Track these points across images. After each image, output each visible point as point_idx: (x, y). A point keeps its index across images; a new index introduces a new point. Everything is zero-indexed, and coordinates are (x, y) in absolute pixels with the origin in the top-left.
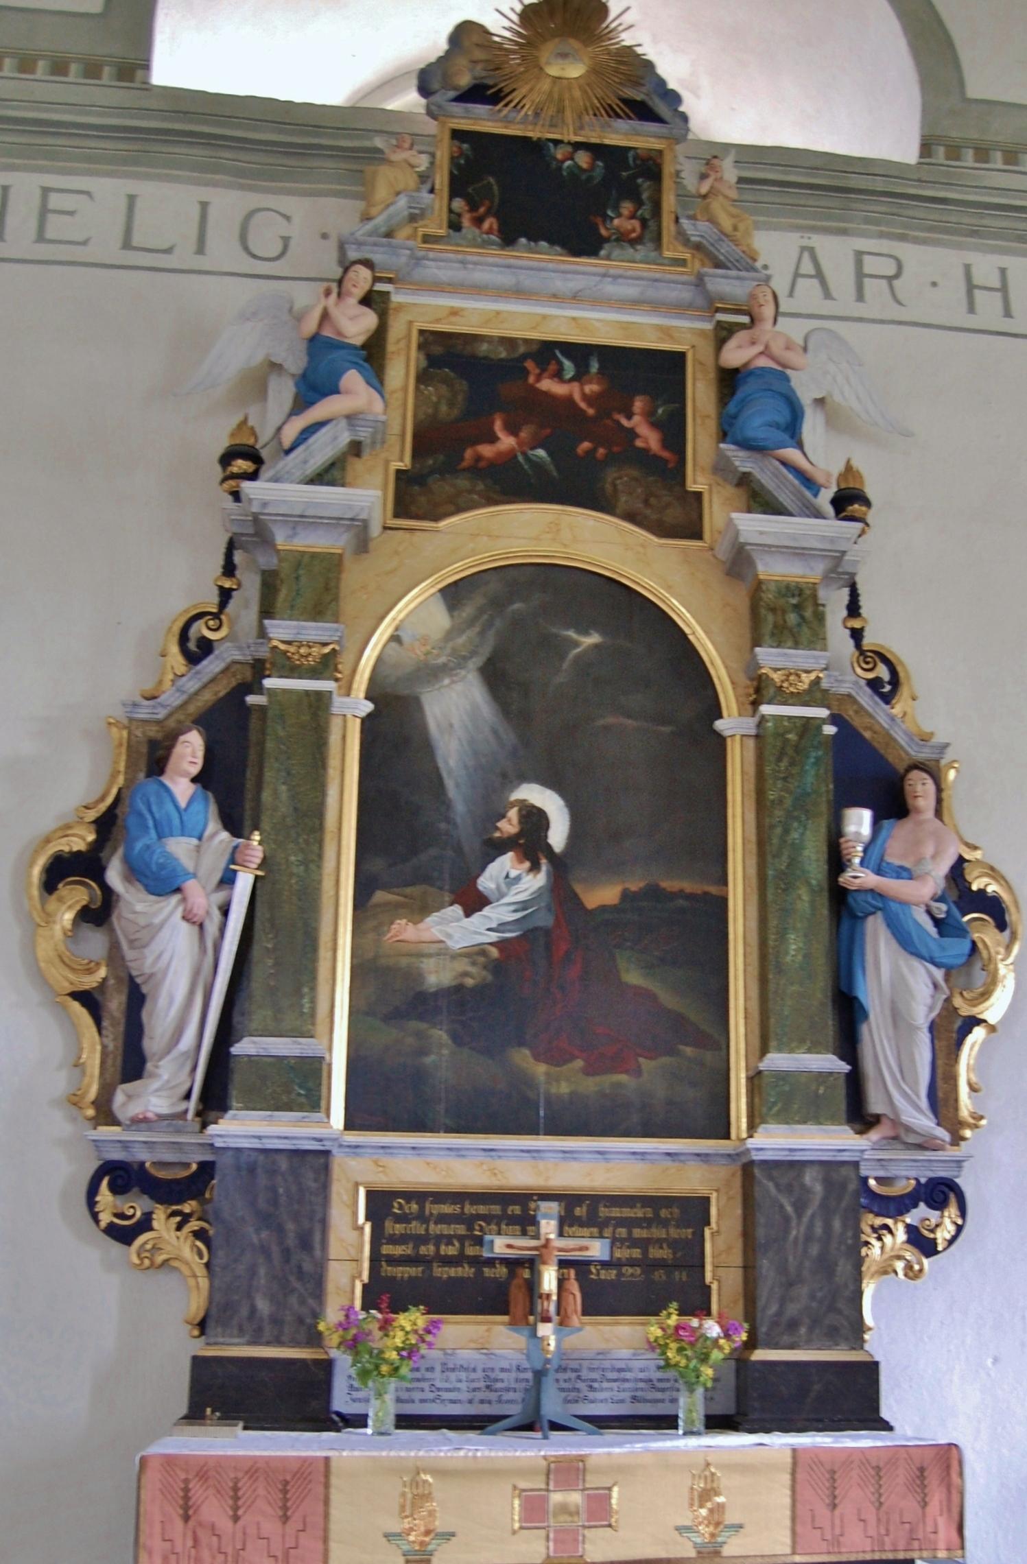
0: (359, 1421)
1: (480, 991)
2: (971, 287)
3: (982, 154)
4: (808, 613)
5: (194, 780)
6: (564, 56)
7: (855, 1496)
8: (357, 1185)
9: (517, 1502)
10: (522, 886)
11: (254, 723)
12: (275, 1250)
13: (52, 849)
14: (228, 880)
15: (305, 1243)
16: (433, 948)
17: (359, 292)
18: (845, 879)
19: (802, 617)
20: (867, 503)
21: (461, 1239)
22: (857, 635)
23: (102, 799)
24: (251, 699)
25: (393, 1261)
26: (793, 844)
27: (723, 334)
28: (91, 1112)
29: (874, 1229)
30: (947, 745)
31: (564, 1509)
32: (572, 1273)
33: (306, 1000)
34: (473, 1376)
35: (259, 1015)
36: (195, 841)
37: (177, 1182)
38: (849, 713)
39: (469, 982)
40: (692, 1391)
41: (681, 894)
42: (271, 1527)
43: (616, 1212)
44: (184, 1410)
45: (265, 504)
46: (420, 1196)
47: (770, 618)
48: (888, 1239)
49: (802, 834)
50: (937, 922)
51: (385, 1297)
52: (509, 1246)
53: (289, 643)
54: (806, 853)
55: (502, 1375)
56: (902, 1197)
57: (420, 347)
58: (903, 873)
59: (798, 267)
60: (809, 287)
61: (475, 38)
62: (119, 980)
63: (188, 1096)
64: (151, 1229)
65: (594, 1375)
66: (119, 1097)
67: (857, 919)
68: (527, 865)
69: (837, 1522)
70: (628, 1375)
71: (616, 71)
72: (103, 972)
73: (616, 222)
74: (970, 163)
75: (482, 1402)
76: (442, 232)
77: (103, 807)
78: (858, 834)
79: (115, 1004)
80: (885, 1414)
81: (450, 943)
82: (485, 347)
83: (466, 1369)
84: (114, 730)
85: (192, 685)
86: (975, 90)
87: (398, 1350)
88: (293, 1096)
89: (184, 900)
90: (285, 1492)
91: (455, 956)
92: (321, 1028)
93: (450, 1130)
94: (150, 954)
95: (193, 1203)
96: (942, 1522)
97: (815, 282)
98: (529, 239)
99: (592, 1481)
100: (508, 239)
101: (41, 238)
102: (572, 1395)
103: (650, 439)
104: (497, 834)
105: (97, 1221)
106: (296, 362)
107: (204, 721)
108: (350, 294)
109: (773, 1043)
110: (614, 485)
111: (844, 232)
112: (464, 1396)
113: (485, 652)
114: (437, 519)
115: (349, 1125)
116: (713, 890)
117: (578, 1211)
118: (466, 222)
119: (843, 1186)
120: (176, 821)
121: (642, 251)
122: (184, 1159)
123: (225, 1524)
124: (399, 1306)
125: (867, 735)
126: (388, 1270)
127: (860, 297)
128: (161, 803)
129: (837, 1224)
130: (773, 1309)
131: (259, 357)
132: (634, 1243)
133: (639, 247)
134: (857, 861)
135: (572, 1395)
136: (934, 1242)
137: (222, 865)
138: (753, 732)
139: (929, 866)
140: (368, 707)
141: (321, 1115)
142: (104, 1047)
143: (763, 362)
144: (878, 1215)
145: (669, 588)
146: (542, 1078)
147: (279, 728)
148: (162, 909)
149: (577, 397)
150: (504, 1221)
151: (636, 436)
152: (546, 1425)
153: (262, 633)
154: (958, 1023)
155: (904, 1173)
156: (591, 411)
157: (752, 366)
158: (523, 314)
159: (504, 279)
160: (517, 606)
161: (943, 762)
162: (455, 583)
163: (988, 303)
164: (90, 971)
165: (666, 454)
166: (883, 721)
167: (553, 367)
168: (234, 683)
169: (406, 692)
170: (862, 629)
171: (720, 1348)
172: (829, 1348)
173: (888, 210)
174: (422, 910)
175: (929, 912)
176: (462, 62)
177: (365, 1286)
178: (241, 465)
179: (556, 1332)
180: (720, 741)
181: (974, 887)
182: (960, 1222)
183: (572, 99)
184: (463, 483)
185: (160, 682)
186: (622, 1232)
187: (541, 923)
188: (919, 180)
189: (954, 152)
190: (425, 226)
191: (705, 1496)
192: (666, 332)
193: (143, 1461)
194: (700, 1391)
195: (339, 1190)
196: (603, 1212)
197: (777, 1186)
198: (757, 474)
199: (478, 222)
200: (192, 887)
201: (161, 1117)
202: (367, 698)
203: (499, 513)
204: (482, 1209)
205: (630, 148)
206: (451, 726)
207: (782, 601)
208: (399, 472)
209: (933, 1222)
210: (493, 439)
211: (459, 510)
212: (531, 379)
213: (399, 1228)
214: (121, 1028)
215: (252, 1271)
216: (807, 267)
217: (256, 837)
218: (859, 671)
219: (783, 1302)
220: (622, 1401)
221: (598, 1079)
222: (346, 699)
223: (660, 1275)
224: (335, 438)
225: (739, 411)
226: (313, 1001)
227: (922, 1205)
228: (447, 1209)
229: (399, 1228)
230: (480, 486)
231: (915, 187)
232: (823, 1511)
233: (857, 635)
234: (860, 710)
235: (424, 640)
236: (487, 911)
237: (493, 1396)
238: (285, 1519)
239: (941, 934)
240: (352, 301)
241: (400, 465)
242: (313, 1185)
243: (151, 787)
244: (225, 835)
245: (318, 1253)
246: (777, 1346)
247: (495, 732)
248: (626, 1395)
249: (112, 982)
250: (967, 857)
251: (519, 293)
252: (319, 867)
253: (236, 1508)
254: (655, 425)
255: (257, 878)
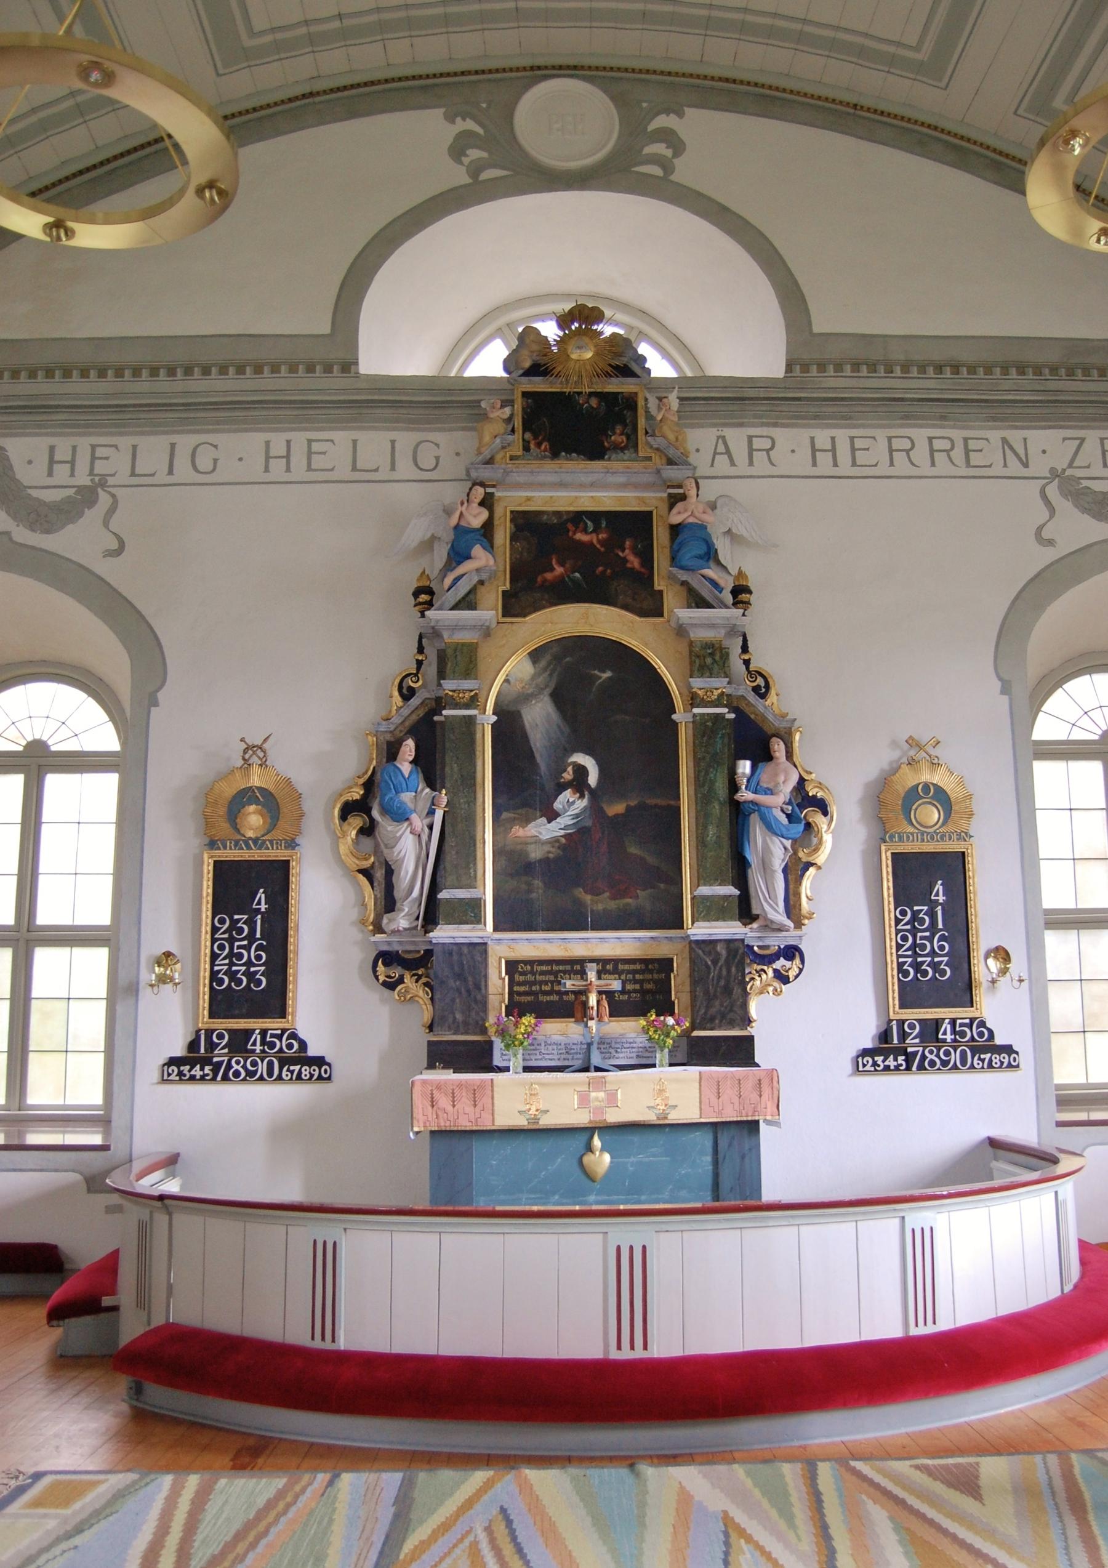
0: (507, 1069)
1: (557, 860)
2: (814, 450)
3: (822, 367)
4: (717, 658)
5: (411, 762)
6: (580, 348)
7: (729, 1093)
8: (500, 958)
9: (576, 1097)
10: (575, 806)
11: (438, 732)
12: (463, 990)
13: (343, 799)
14: (431, 813)
15: (478, 987)
16: (533, 840)
17: (478, 500)
18: (738, 797)
19: (714, 659)
20: (750, 592)
21: (552, 982)
22: (747, 663)
23: (366, 772)
24: (436, 718)
25: (519, 994)
26: (710, 780)
27: (675, 500)
28: (371, 928)
29: (757, 972)
30: (795, 719)
31: (597, 1099)
32: (604, 997)
33: (472, 871)
34: (560, 1047)
35: (451, 879)
36: (414, 794)
37: (414, 959)
38: (743, 706)
39: (551, 856)
40: (662, 1051)
41: (656, 806)
42: (469, 1109)
43: (627, 967)
44: (426, 1066)
45: (438, 621)
46: (530, 962)
47: (697, 661)
48: (764, 976)
49: (715, 775)
50: (788, 816)
51: (516, 1010)
52: (573, 985)
53: (454, 691)
54: (717, 784)
55: (574, 1047)
56: (771, 955)
57: (512, 520)
58: (770, 792)
59: (716, 449)
60: (722, 461)
61: (532, 337)
62: (380, 863)
63: (418, 918)
64: (404, 982)
65: (618, 1046)
66: (385, 921)
67: (746, 816)
68: (578, 795)
69: (721, 1104)
70: (634, 1045)
71: (609, 351)
72: (372, 859)
73: (613, 438)
74: (815, 374)
75: (564, 1059)
76: (520, 453)
77: (367, 777)
78: (744, 773)
79: (379, 874)
80: (756, 1060)
81: (541, 837)
82: (545, 517)
83: (557, 1044)
84: (369, 737)
85: (406, 712)
86: (816, 329)
87: (523, 1034)
88: (468, 917)
89: (411, 824)
90: (474, 1094)
91: (544, 843)
92: (479, 882)
93: (544, 930)
94: (396, 850)
95: (423, 969)
96: (769, 1104)
97: (726, 456)
98: (566, 453)
99: (609, 1087)
100: (555, 455)
101: (309, 468)
102: (606, 1055)
103: (634, 562)
104: (562, 780)
105: (378, 980)
106: (448, 536)
107: (413, 731)
108: (473, 502)
109: (702, 882)
110: (616, 589)
111: (741, 425)
112: (556, 1057)
113: (552, 685)
114: (525, 616)
115: (496, 929)
116: (672, 803)
117: (608, 967)
118: (532, 446)
119: (737, 951)
120: (404, 785)
121: (627, 454)
122: (417, 949)
123: (449, 1108)
124: (521, 1015)
125: (752, 716)
126: (517, 998)
127: (751, 463)
128: (396, 777)
129: (733, 970)
130: (703, 1011)
131: (429, 535)
132: (636, 982)
133: (626, 452)
134: (743, 787)
135: (606, 1055)
136: (788, 977)
137: (428, 806)
138: (691, 720)
139: (782, 787)
140: (495, 718)
141: (481, 926)
142: (375, 896)
143: (691, 520)
144: (758, 964)
145: (646, 645)
146: (589, 902)
147: (451, 735)
148: (400, 829)
149: (595, 541)
150: (570, 973)
151: (627, 561)
152: (592, 1069)
153: (440, 685)
154: (801, 866)
155: (772, 943)
156: (602, 549)
157: (686, 522)
158: (564, 497)
159: (552, 478)
160: (568, 659)
161: (793, 729)
162: (536, 649)
163: (824, 459)
164: (366, 859)
165: (643, 570)
166: (761, 709)
167: (581, 525)
168: (427, 709)
169: (514, 709)
170: (750, 659)
171: (674, 1030)
172: (730, 1029)
173: (769, 409)
174: (527, 821)
175: (782, 811)
176: (525, 352)
177: (506, 1007)
178: (424, 598)
179: (597, 1025)
180: (675, 725)
181: (810, 794)
182: (801, 966)
183: (586, 370)
184: (538, 595)
185: (390, 711)
186: (630, 976)
187: (587, 825)
188: (785, 388)
189: (805, 368)
190: (511, 451)
191: (661, 1091)
192: (642, 500)
193: (413, 1082)
194: (666, 1050)
195: (492, 961)
196: (621, 967)
197: (703, 951)
198: (690, 581)
199: (539, 445)
200: (414, 817)
201: (405, 929)
202: (493, 714)
203: (556, 611)
204: (561, 968)
205: (618, 393)
206: (537, 725)
207: (702, 652)
208: (504, 592)
209: (788, 967)
210: (552, 569)
211: (536, 610)
212: (571, 534)
213: (522, 978)
214: (383, 886)
215: (453, 1000)
216: (721, 448)
217: (444, 791)
218: (748, 682)
219: (708, 1007)
220: (632, 1058)
221: (617, 901)
222: (484, 716)
223: (649, 997)
224: (471, 580)
225: (679, 549)
226: (475, 871)
227: (782, 958)
228: (544, 968)
229: (522, 978)
230: (546, 596)
231: (783, 392)
232: (714, 1099)
233: (747, 663)
234: (749, 704)
235: (521, 681)
236: (558, 820)
237: (570, 1057)
238: (475, 1106)
239: (790, 822)
240: (475, 505)
241: (504, 588)
242: (479, 959)
243: (390, 768)
244: (428, 790)
245: (483, 991)
246: (704, 1029)
247: (559, 727)
248: (634, 1055)
249: (377, 864)
250: (806, 778)
251: (562, 485)
252: (475, 804)
253: (453, 1101)
254: (636, 554)
255: (445, 812)
